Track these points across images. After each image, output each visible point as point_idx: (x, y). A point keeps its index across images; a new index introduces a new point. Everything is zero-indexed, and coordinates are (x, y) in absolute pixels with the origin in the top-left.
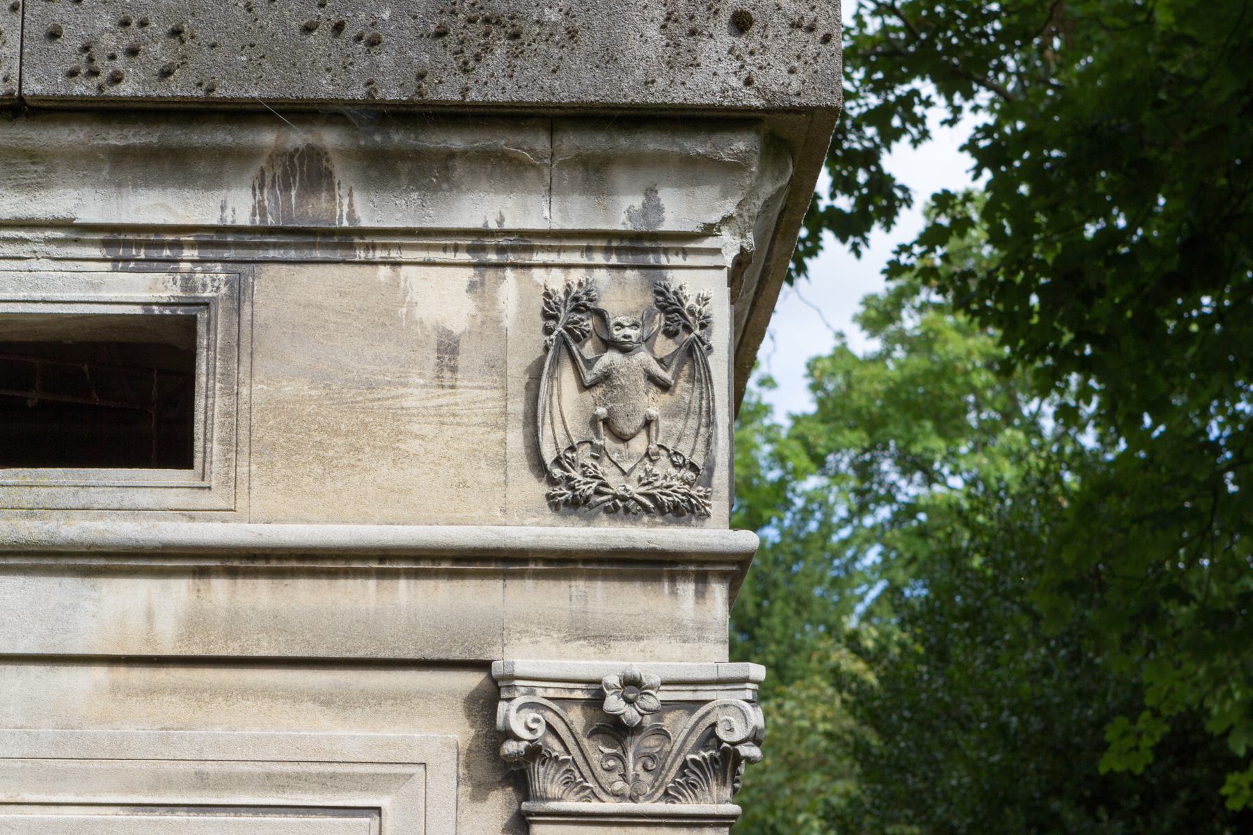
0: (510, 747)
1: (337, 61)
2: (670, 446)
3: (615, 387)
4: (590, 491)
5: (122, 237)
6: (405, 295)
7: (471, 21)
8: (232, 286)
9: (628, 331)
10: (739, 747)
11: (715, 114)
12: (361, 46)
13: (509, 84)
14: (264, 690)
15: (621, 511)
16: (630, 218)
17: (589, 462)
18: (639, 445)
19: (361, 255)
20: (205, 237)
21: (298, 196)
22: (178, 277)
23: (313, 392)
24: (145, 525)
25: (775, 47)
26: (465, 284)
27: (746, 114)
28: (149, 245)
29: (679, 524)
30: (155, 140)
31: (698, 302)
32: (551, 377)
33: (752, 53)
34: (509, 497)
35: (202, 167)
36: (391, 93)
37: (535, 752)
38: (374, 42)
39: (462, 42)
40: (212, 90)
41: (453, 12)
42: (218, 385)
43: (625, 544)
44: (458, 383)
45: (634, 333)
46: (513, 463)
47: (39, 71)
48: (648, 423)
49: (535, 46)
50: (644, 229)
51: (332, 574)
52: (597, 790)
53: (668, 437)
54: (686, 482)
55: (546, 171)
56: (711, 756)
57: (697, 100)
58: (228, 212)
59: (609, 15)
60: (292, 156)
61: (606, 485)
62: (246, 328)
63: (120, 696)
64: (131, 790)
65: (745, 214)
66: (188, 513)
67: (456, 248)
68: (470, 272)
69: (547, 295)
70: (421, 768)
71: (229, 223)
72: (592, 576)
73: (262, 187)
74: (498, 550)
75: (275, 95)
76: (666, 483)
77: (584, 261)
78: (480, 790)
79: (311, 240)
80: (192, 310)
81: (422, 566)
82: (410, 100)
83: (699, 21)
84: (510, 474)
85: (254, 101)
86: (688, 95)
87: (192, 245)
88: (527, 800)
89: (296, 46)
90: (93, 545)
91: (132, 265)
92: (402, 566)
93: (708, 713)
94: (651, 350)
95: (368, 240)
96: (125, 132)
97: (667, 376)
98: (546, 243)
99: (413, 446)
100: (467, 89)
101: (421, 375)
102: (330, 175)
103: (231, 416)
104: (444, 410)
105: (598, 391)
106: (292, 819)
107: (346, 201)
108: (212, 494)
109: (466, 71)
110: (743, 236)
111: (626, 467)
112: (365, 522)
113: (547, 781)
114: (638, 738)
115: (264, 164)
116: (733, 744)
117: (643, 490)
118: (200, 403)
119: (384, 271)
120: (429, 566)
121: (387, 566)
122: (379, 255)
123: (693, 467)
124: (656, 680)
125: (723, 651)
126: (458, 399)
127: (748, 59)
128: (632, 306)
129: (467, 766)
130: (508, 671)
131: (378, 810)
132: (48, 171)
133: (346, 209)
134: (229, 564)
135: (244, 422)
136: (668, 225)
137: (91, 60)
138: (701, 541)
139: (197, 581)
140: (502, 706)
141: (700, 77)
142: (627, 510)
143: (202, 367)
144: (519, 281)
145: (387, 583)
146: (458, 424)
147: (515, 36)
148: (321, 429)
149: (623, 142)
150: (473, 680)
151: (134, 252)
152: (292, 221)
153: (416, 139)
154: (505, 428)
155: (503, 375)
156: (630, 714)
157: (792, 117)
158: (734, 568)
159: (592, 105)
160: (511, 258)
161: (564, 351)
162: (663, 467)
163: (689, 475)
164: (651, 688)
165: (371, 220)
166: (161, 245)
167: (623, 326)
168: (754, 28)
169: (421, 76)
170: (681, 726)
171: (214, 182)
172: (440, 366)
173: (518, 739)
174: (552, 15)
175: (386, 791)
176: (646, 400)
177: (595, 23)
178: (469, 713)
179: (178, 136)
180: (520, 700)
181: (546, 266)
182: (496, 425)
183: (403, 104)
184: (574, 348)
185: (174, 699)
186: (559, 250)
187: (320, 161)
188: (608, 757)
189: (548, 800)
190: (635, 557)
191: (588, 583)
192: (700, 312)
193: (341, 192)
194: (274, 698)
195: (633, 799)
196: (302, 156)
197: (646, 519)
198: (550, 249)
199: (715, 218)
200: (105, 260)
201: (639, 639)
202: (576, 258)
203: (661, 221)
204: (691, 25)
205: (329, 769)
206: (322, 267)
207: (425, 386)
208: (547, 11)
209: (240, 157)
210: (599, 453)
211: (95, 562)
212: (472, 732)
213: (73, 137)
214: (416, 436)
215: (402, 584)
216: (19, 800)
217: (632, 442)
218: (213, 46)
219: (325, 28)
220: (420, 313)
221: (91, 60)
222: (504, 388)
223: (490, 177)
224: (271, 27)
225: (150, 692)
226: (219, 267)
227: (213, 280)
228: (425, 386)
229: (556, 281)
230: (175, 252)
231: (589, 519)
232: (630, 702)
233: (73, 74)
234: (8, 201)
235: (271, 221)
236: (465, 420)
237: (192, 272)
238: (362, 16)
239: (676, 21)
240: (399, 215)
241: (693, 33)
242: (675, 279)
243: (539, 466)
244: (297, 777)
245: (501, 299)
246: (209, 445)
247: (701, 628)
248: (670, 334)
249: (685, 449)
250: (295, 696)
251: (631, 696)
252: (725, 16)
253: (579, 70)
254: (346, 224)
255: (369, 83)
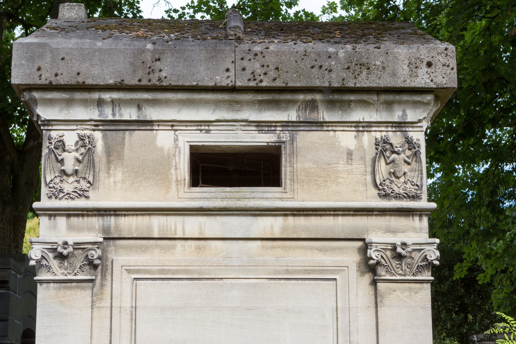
0: (372, 262)
1: (320, 76)
2: (411, 180)
3: (396, 164)
4: (390, 192)
5: (261, 124)
6: (338, 139)
7: (356, 65)
8: (291, 137)
9: (399, 149)
10: (433, 261)
11: (422, 89)
12: (327, 72)
13: (367, 82)
14: (303, 247)
15: (398, 198)
16: (398, 118)
17: (389, 184)
18: (402, 179)
19: (325, 128)
20: (284, 124)
21: (309, 112)
22: (276, 135)
23: (314, 166)
24: (271, 202)
25: (439, 71)
26: (354, 136)
27: (430, 90)
28: (268, 126)
29: (414, 201)
30: (271, 98)
31: (417, 140)
32: (378, 161)
33: (432, 73)
34: (368, 194)
35: (283, 105)
36: (335, 84)
37: (378, 263)
38: (330, 71)
39: (354, 70)
40: (287, 84)
41: (351, 62)
42: (288, 164)
43: (400, 207)
44: (353, 163)
45: (401, 149)
46: (368, 185)
47: (240, 79)
48: (405, 174)
49: (374, 71)
50: (402, 121)
51: (321, 215)
52: (395, 273)
53: (410, 178)
54: (416, 190)
55: (376, 105)
56: (425, 264)
57: (418, 86)
58: (290, 117)
59: (393, 63)
60: (307, 102)
61: (394, 191)
62: (295, 149)
63: (264, 249)
64: (269, 274)
65: (429, 117)
66: (281, 199)
67: (351, 126)
68: (355, 133)
69: (376, 139)
70: (347, 268)
71: (290, 120)
72: (391, 215)
73: (299, 110)
74: (366, 208)
75: (304, 85)
76: (410, 190)
77: (386, 129)
78: (363, 273)
79: (312, 124)
80: (280, 144)
81: (345, 213)
82: (341, 86)
83: (418, 64)
84: (368, 188)
85: (298, 87)
86: (416, 84)
87: (280, 126)
88: (376, 276)
89: (309, 72)
90: (257, 208)
91: (264, 132)
92: (340, 213)
93: (424, 252)
94: (405, 154)
95: (327, 124)
96: (263, 96)
97: (410, 161)
98: (376, 125)
99: (341, 180)
100: (356, 83)
101: (343, 161)
102: (317, 107)
103: (292, 173)
104: (349, 171)
105: (391, 165)
106: (312, 282)
107: (322, 114)
108: (287, 194)
109: (355, 78)
110: (428, 122)
111: (399, 186)
112: (329, 201)
113: (381, 271)
114: (405, 259)
115: (300, 104)
116: (432, 260)
117: (404, 192)
118: (283, 169)
119: (332, 133)
120: (347, 213)
121: (336, 213)
122: (330, 128)
123: (417, 185)
124: (410, 243)
125: (427, 235)
126: (353, 167)
127: (431, 74)
128: (399, 142)
129: (359, 267)
130: (370, 241)
131: (335, 279)
132: (241, 107)
133: (322, 116)
134: (293, 213)
135: (295, 174)
136: (409, 120)
137: (254, 76)
138: (421, 205)
139: (284, 218)
140: (369, 251)
141: (419, 79)
142: (400, 197)
143: (283, 159)
144: (368, 135)
145: (336, 218)
146: (353, 174)
147: (368, 69)
148: (316, 176)
149: (397, 97)
150: (360, 244)
151: (264, 128)
152: (307, 119)
153: (341, 97)
154: (366, 175)
155: (365, 161)
156: (404, 253)
157: (442, 90)
158: (430, 213)
159: (389, 87)
160: (366, 129)
161: (382, 154)
162: (409, 185)
163: (416, 188)
164: (409, 245)
165: (328, 119)
166: (271, 126)
167: (397, 147)
168: (433, 66)
169: (343, 80)
170: (417, 255)
171: (286, 109)
172: (348, 159)
173: (374, 260)
174: (378, 63)
175: (337, 274)
176: (404, 167)
177: (390, 65)
178: (359, 253)
179: (277, 97)
180: (374, 249)
181: (375, 131)
182: (363, 174)
183: (338, 87)
184: (384, 153)
185: (279, 249)
186: (379, 127)
187: (315, 103)
188: (397, 264)
189: (381, 276)
190: (403, 210)
191: (390, 217)
192: (418, 143)
193: (321, 112)
194: (306, 249)
195: (404, 276)
196: (310, 102)
197: (405, 199)
198: (377, 126)
199: (421, 118)
200: (256, 130)
201: (404, 232)
202: (383, 129)
203: (407, 118)
204: (416, 65)
205: (322, 268)
206: (315, 132)
207: (344, 164)
208: (377, 62)
209: (293, 102)
210: (392, 182)
211: (257, 213)
212: (360, 258)
213: (249, 97)
214: (342, 178)
215: (340, 218)
216: (238, 277)
217: (400, 179)
218: (287, 72)
219: (317, 67)
220: (342, 144)
221: (254, 76)
222: (365, 164)
223: (361, 107)
224: (302, 67)
225: (273, 248)
226: (287, 132)
227: (286, 136)
228: (344, 164)
229: (378, 135)
230: (275, 128)
231: (390, 200)
232: (403, 249)
233: (249, 80)
234: (230, 115)
235: (301, 120)
236: (355, 173)
237: (280, 133)
238: (327, 64)
239: (412, 64)
240: (336, 118)
241: (416, 67)
242: (410, 134)
243: (376, 185)
244: (313, 270)
245: (364, 140)
246: (286, 181)
247: (421, 229)
248: (410, 149)
249: (415, 180)
250: (311, 249)
251: (404, 248)
252: (425, 63)
253: (386, 78)
254: (322, 120)
255: (330, 82)
